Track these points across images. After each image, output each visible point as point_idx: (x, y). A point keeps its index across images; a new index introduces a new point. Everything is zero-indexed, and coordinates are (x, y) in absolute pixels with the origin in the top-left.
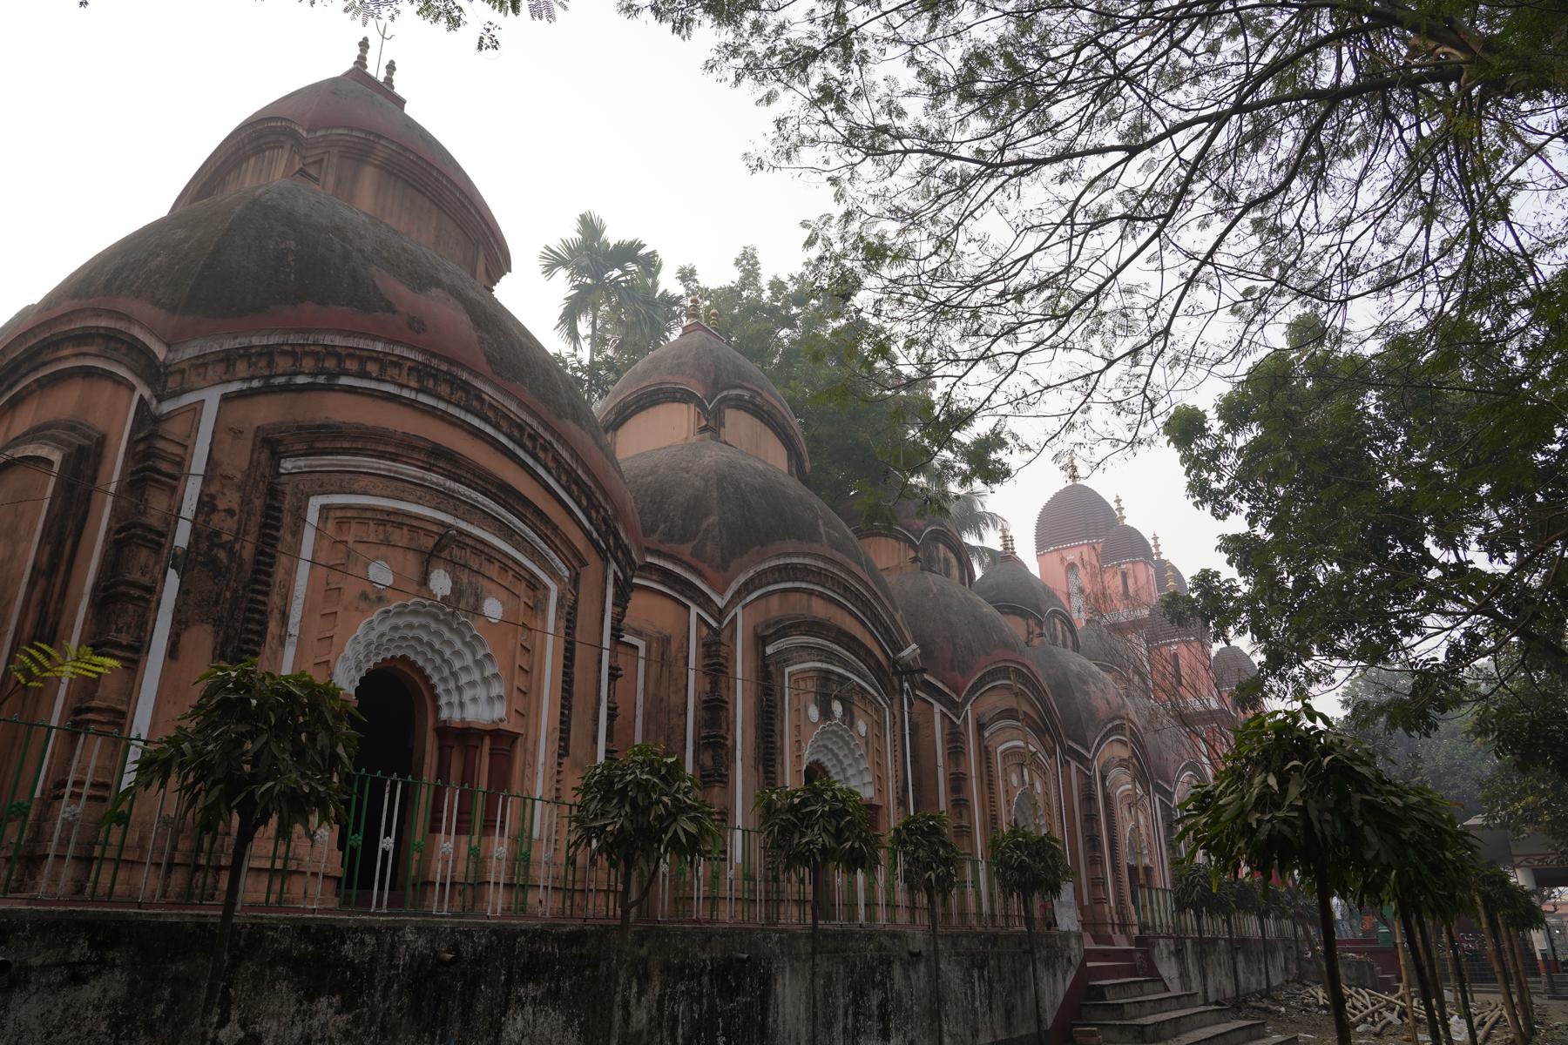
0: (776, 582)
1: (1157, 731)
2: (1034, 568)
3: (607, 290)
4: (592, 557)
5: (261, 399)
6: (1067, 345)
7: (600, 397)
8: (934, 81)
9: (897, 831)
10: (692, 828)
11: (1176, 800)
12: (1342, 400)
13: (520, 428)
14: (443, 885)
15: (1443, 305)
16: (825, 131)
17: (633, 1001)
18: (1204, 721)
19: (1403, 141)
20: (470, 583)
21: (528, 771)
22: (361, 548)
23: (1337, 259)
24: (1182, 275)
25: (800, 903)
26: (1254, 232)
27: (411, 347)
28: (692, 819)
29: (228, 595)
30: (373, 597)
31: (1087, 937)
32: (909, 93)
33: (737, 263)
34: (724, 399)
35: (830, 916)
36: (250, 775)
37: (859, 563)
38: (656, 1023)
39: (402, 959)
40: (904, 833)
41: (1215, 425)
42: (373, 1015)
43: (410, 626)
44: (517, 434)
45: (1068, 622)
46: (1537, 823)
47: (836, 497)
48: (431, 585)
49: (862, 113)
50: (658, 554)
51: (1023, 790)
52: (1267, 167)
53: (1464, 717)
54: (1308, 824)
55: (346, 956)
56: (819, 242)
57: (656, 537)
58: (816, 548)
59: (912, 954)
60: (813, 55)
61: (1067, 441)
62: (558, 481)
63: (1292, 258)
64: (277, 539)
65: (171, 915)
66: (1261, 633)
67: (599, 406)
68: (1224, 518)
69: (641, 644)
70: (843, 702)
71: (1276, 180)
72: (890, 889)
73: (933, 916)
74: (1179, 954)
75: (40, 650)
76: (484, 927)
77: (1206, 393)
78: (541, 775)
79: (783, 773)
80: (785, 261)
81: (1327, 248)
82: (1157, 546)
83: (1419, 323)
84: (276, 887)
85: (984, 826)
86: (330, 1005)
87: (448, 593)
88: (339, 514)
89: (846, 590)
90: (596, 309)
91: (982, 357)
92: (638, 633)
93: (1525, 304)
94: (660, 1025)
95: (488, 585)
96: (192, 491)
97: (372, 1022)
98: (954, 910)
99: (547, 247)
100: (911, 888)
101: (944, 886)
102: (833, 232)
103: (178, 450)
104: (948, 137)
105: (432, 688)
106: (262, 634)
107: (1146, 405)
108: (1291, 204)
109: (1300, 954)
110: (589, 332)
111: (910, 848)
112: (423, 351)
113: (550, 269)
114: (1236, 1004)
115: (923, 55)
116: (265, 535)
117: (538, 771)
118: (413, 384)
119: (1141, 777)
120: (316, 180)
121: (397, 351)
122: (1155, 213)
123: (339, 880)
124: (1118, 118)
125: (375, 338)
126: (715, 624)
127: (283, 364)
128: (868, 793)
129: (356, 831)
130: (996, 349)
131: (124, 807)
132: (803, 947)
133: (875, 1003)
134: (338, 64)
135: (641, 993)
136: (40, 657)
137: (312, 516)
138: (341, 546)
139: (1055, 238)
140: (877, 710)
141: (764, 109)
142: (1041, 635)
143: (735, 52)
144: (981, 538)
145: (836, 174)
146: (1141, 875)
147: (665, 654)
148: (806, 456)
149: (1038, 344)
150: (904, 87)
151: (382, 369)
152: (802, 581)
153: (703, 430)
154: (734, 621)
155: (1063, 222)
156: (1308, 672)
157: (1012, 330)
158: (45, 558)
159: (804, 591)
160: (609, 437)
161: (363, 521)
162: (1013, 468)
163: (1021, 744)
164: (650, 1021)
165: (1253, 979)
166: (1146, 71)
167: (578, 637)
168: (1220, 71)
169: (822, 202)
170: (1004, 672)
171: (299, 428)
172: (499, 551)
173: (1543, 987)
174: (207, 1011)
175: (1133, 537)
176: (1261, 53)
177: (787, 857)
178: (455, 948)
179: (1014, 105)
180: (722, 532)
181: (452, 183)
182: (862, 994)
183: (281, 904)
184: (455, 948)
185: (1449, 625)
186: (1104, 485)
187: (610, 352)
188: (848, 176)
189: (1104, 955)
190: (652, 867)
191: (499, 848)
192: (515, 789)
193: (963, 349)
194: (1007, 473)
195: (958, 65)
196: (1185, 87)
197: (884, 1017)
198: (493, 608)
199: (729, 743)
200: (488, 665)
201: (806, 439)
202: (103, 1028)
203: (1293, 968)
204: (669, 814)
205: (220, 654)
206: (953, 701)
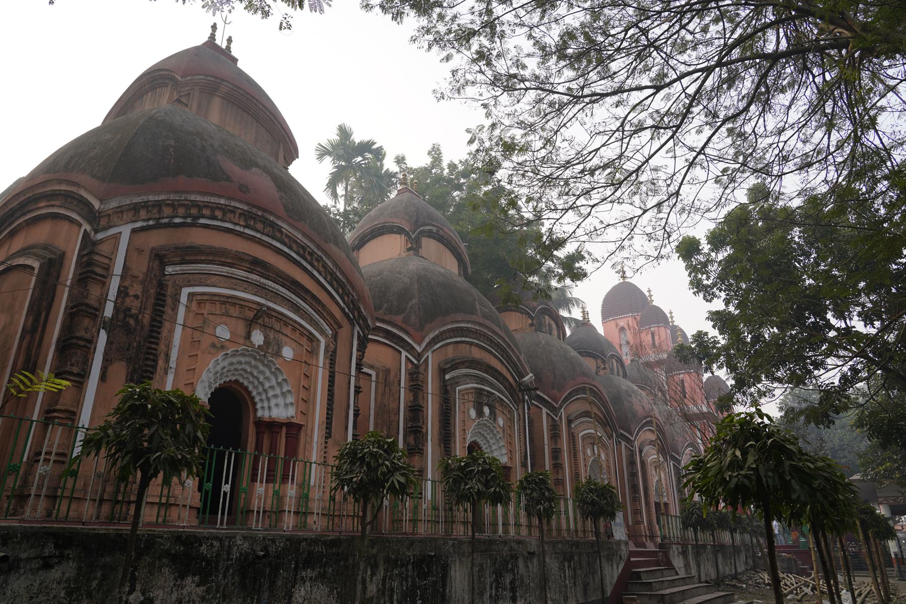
0: (451, 337)
1: (671, 424)
2: (601, 330)
3: (354, 169)
6: (619, 201)
8: (543, 48)
10: (402, 480)
11: (683, 464)
12: (779, 233)
13: (304, 248)
14: (258, 512)
15: (838, 178)
16: (480, 77)
17: (368, 579)
18: (699, 419)
19: (815, 83)
20: (274, 338)
21: (308, 447)
22: (211, 318)
23: (776, 151)
24: (686, 160)
25: (465, 523)
27: (241, 202)
28: (403, 475)
29: (135, 344)
30: (218, 346)
31: (631, 543)
32: (529, 55)
33: (429, 153)
35: (482, 531)
38: (381, 592)
39: (235, 555)
40: (525, 483)
41: (705, 247)
42: (218, 587)
43: (240, 363)
44: (301, 252)
45: (620, 361)
46: (892, 478)
47: (486, 289)
49: (502, 66)
51: (593, 458)
52: (736, 98)
53: (850, 417)
54: (759, 478)
56: (477, 141)
57: (382, 311)
59: (529, 553)
61: (619, 257)
62: (325, 279)
63: (750, 151)
64: (163, 312)
65: (102, 529)
66: (732, 368)
67: (349, 236)
69: (373, 373)
70: (491, 407)
71: (741, 105)
72: (517, 515)
73: (541, 531)
74: (684, 553)
76: (282, 537)
77: (700, 229)
80: (457, 152)
81: (771, 145)
82: (672, 317)
83: (824, 189)
84: (162, 513)
86: (193, 582)
88: (199, 298)
89: (491, 342)
90: (347, 179)
91: (571, 208)
92: (372, 367)
93: (885, 178)
94: (384, 594)
95: (285, 339)
96: (114, 284)
97: (217, 591)
99: (319, 144)
100: (529, 515)
101: (548, 514)
102: (485, 136)
103: (106, 261)
105: (252, 398)
106: (154, 367)
107: (666, 236)
108: (750, 120)
109: (754, 553)
111: (529, 491)
112: (248, 204)
113: (321, 157)
114: (717, 583)
115: (537, 33)
116: (156, 310)
117: (314, 446)
120: (187, 105)
122: (672, 124)
123: (198, 509)
125: (220, 196)
126: (416, 362)
127: (167, 211)
128: (504, 460)
129: (208, 481)
130: (578, 203)
131: (75, 467)
132: (466, 548)
133: (508, 581)
134: (199, 38)
135: (372, 575)
137: (184, 299)
139: (613, 139)
140: (509, 412)
141: (444, 64)
142: (605, 368)
143: (428, 32)
144: (570, 312)
145: (486, 102)
147: (387, 380)
148: (469, 265)
149: (603, 200)
150: (526, 52)
151: (224, 214)
153: (409, 249)
155: (618, 130)
156: (759, 390)
158: (29, 324)
159: (467, 343)
160: (355, 254)
161: (213, 302)
162: (589, 272)
163: (593, 431)
164: (378, 591)
165: (727, 569)
166: (666, 42)
168: (708, 43)
169: (478, 118)
170: (583, 390)
171: (176, 248)
173: (895, 574)
174: (122, 585)
175: (658, 312)
176: (733, 32)
177: (457, 496)
178: (265, 549)
180: (433, 305)
181: (265, 107)
182: (501, 576)
184: (265, 549)
185: (841, 363)
186: (641, 282)
187: (356, 205)
188: (493, 103)
189: (641, 554)
190: (379, 502)
191: (291, 491)
192: (301, 457)
193: (560, 203)
194: (585, 275)
195: (557, 39)
196: (689, 52)
197: (513, 589)
198: (288, 352)
199: (424, 430)
200: (284, 385)
201: (469, 255)
202: (62, 595)
203: (751, 562)
204: (389, 471)
205: (130, 379)
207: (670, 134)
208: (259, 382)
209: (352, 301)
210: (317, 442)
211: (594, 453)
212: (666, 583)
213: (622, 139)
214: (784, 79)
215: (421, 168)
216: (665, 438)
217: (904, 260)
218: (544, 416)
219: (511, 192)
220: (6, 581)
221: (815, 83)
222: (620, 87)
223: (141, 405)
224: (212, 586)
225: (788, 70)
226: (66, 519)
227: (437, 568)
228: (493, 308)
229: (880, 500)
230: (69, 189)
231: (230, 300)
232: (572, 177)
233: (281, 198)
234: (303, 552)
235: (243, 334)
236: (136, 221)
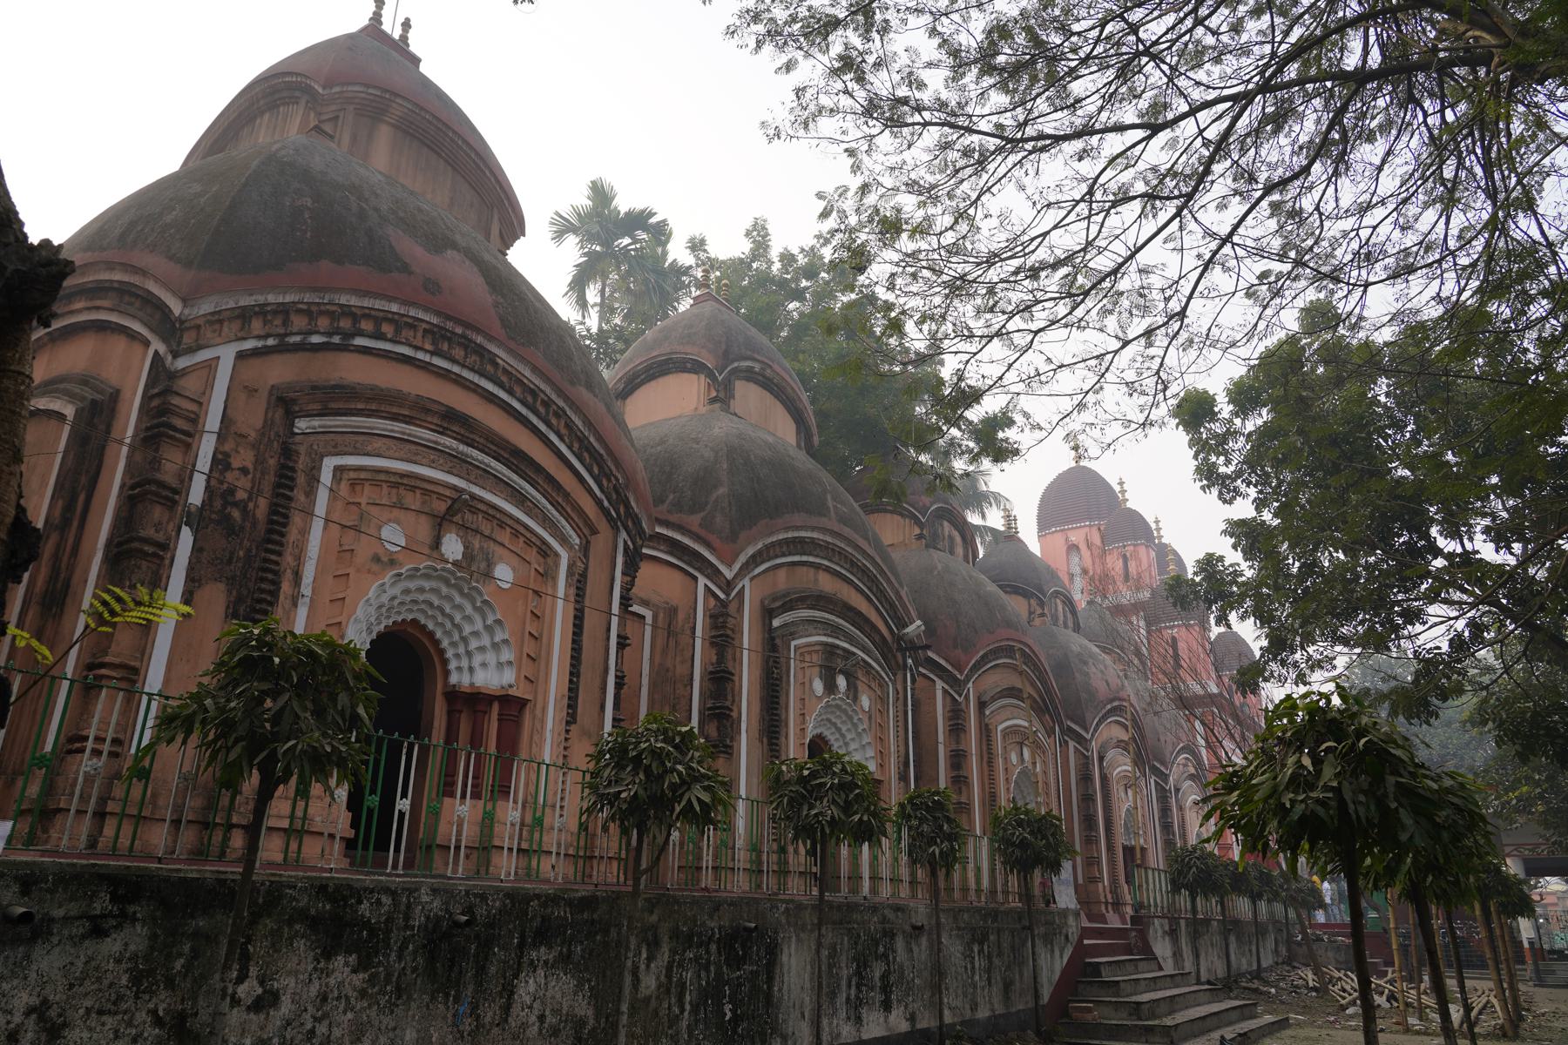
0: (784, 555)
1: (1156, 713)
2: (1034, 546)
3: (616, 258)
6: (1081, 325)
7: (608, 367)
8: (955, 53)
9: (902, 805)
10: (706, 798)
12: (1352, 388)
13: (533, 393)
14: (458, 848)
16: (845, 101)
17: (643, 967)
19: (1426, 125)
20: (481, 548)
21: (536, 738)
22: (374, 510)
23: (1355, 245)
24: (1199, 256)
26: (1272, 215)
27: (426, 309)
28: (706, 789)
30: (385, 559)
32: (930, 65)
33: (748, 234)
34: (735, 371)
36: (271, 733)
37: (866, 539)
38: (664, 989)
41: (1224, 408)
42: (389, 975)
43: (421, 590)
44: (530, 399)
45: (1069, 603)
46: (1530, 813)
47: (842, 476)
48: (443, 549)
49: (882, 83)
50: (667, 524)
51: (1019, 768)
52: (1288, 150)
53: (1462, 706)
54: (1342, 802)
55: (363, 916)
56: (834, 214)
57: (665, 507)
59: (915, 928)
60: (834, 24)
61: (1076, 422)
62: (570, 448)
63: (1310, 242)
64: (290, 499)
65: (191, 871)
66: (1263, 616)
68: (1230, 503)
69: (648, 614)
70: (849, 676)
74: (1173, 933)
76: (498, 890)
77: (1218, 376)
78: (549, 741)
79: (787, 746)
80: (797, 232)
81: (1345, 234)
82: (1158, 529)
83: (1436, 311)
85: (983, 803)
86: (346, 964)
87: (460, 557)
88: (352, 475)
89: (853, 565)
90: (604, 277)
91: (998, 334)
92: (645, 603)
94: (668, 991)
95: (499, 550)
97: (388, 981)
99: (557, 214)
100: (913, 862)
101: (949, 860)
102: (849, 204)
103: (192, 407)
104: (969, 110)
105: (442, 652)
106: (275, 594)
108: (1311, 188)
109: (1290, 936)
110: (598, 300)
111: (915, 823)
112: (438, 313)
113: (559, 235)
114: (1226, 985)
115: (945, 26)
116: (278, 495)
117: (546, 735)
118: (428, 347)
119: (1139, 761)
120: (332, 137)
122: (1179, 191)
125: (391, 299)
126: (722, 596)
127: (299, 322)
129: (373, 792)
131: (146, 763)
132: (809, 917)
133: (877, 974)
134: (353, 20)
135: (650, 959)
136: (113, 602)
137: (326, 476)
138: (354, 508)
140: (880, 686)
141: (783, 77)
142: (1043, 615)
143: (756, 18)
144: (984, 517)
145: (853, 145)
146: (1138, 855)
147: (672, 626)
148: (815, 430)
149: (1053, 323)
150: (925, 58)
151: (398, 331)
152: (810, 554)
153: (713, 401)
155: (1082, 200)
156: (1310, 658)
157: (1028, 308)
158: (57, 512)
159: (811, 564)
161: (376, 484)
164: (659, 987)
165: (1244, 961)
166: (1169, 48)
167: (587, 603)
168: (1245, 51)
169: (837, 173)
170: (1009, 651)
171: (314, 388)
172: (511, 516)
173: (1528, 974)
174: (226, 967)
175: (1136, 519)
176: (1286, 33)
178: (469, 910)
179: (1034, 79)
180: (752, 500)
181: (468, 144)
183: (297, 863)
184: (469, 910)
185: (1455, 614)
186: (1108, 468)
187: (617, 321)
188: (865, 147)
189: (1100, 933)
190: (664, 834)
191: (511, 813)
193: (977, 326)
194: (1016, 452)
196: (1207, 66)
197: (886, 989)
199: (735, 715)
200: (498, 630)
202: (124, 981)
203: (1283, 950)
204: (683, 782)
205: (232, 613)
208: (454, 625)
210: (553, 731)
211: (1023, 760)
214: (1373, 118)
216: (1143, 737)
218: (939, 694)
219: (889, 307)
220: (27, 957)
221: (1426, 125)
223: (262, 658)
224: (377, 973)
225: (1381, 103)
231: (405, 481)
232: (1002, 281)
233: (496, 305)
235: (428, 540)
236: (244, 339)
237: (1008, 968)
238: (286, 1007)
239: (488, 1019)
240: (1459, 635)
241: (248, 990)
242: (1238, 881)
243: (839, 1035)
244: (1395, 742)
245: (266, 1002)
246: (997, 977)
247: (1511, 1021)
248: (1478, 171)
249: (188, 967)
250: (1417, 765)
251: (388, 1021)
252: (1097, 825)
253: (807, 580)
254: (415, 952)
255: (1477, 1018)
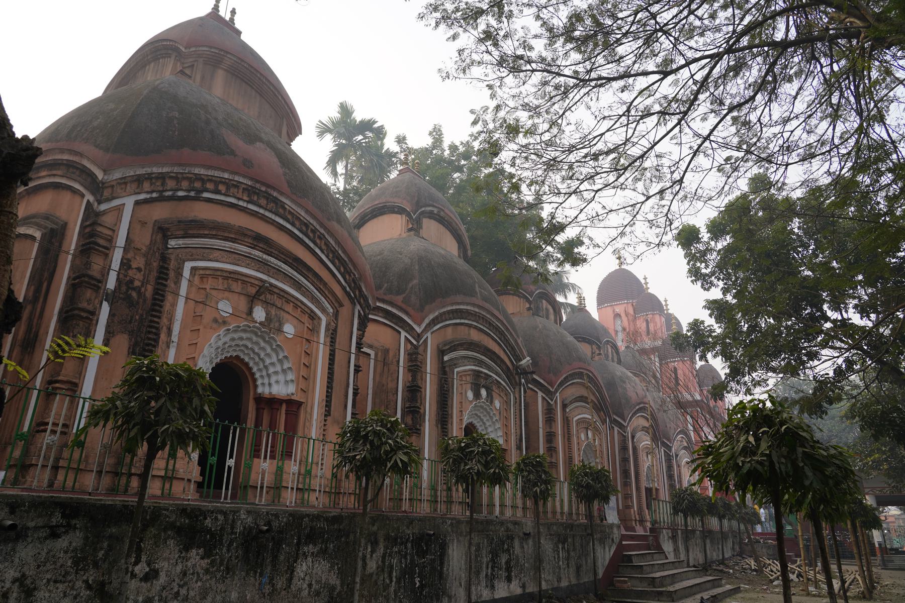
0: (450, 319)
1: (665, 411)
2: (595, 315)
4: (346, 302)
5: (158, 204)
6: (622, 187)
7: (349, 210)
8: (550, 30)
9: (518, 464)
10: (405, 459)
12: (778, 224)
13: (306, 225)
14: (262, 487)
15: (841, 170)
16: (487, 57)
17: (368, 556)
19: (822, 73)
20: (276, 314)
21: (307, 424)
22: (214, 293)
23: (781, 142)
24: (691, 148)
26: (733, 124)
27: (245, 176)
28: (405, 454)
29: (137, 317)
30: (220, 321)
32: (536, 36)
33: (430, 134)
34: (423, 213)
37: (499, 310)
38: (381, 569)
39: (239, 529)
40: (522, 465)
41: (705, 236)
42: (222, 561)
43: (241, 339)
44: (304, 228)
45: (615, 347)
46: (880, 469)
47: (484, 273)
49: (508, 47)
51: (586, 442)
52: (742, 86)
53: (843, 406)
54: (772, 463)
56: (480, 122)
57: (381, 291)
58: (474, 300)
59: (525, 534)
60: (480, 12)
61: (619, 244)
62: (327, 257)
63: (755, 140)
64: (166, 286)
65: (108, 500)
66: (726, 355)
67: (350, 215)
69: (372, 353)
70: (488, 389)
74: (674, 538)
75: (63, 339)
76: (285, 512)
77: (701, 217)
80: (459, 133)
81: (775, 135)
82: (667, 305)
83: (827, 180)
84: (167, 486)
85: (565, 462)
86: (198, 554)
88: (201, 272)
89: (490, 325)
90: (347, 158)
91: (575, 192)
93: (890, 170)
94: (383, 570)
95: (286, 316)
97: (221, 564)
98: (549, 510)
99: (320, 121)
100: (525, 496)
101: (545, 495)
102: (489, 117)
103: (109, 232)
105: (253, 374)
106: (157, 341)
108: (755, 109)
109: (741, 540)
110: (344, 172)
111: (526, 474)
112: (251, 179)
114: (705, 568)
115: (545, 14)
116: (159, 283)
117: (313, 422)
118: (245, 198)
119: (655, 439)
120: (190, 77)
121: (236, 178)
122: (679, 110)
124: (657, 55)
125: (224, 171)
126: (415, 343)
127: (171, 184)
129: (213, 455)
130: (582, 188)
131: (82, 438)
132: (464, 528)
133: (504, 561)
135: (372, 552)
137: (186, 273)
138: (203, 291)
139: (618, 125)
140: (506, 395)
141: (451, 43)
142: (600, 354)
143: (436, 9)
144: (566, 297)
145: (491, 82)
147: (386, 360)
148: (469, 247)
149: (606, 186)
150: (533, 32)
151: (228, 189)
153: (410, 230)
154: (426, 341)
155: (623, 115)
156: (753, 379)
158: (31, 294)
161: (215, 277)
164: (378, 568)
165: (714, 554)
166: (674, 27)
168: (718, 29)
169: (482, 99)
170: (580, 375)
171: (179, 222)
172: (293, 296)
174: (128, 556)
176: (742, 19)
177: (456, 477)
178: (268, 523)
179: (596, 45)
180: (432, 287)
181: (269, 81)
182: (497, 556)
183: (170, 496)
184: (268, 523)
185: (837, 354)
186: (638, 270)
187: (355, 184)
189: (632, 538)
191: (292, 467)
193: (563, 187)
194: (585, 260)
195: (565, 20)
196: (696, 38)
197: (509, 569)
198: (289, 329)
199: (422, 411)
200: (285, 362)
202: (69, 564)
203: (737, 548)
204: (392, 450)
205: (132, 352)
206: (550, 391)
207: (675, 121)
208: (260, 359)
209: (353, 280)
211: (588, 438)
212: (656, 567)
213: (627, 125)
214: (791, 68)
215: (422, 149)
217: (901, 254)
218: (540, 400)
219: (512, 176)
220: (14, 549)
221: (822, 73)
222: (625, 72)
223: (149, 377)
225: (796, 59)
226: (63, 489)
227: (435, 547)
228: (492, 291)
229: (867, 490)
230: (71, 158)
231: (232, 276)
232: (577, 161)
234: (306, 527)
237: (579, 557)
238: (163, 579)
239: (279, 586)
240: (840, 367)
241: (141, 569)
242: (712, 508)
243: (481, 596)
244: (802, 428)
245: (151, 576)
246: (573, 563)
247: (868, 589)
248: (852, 99)
249: (106, 555)
250: (815, 442)
251: (221, 587)
252: (630, 474)
253: (464, 334)
254: (237, 547)
255: (848, 587)
